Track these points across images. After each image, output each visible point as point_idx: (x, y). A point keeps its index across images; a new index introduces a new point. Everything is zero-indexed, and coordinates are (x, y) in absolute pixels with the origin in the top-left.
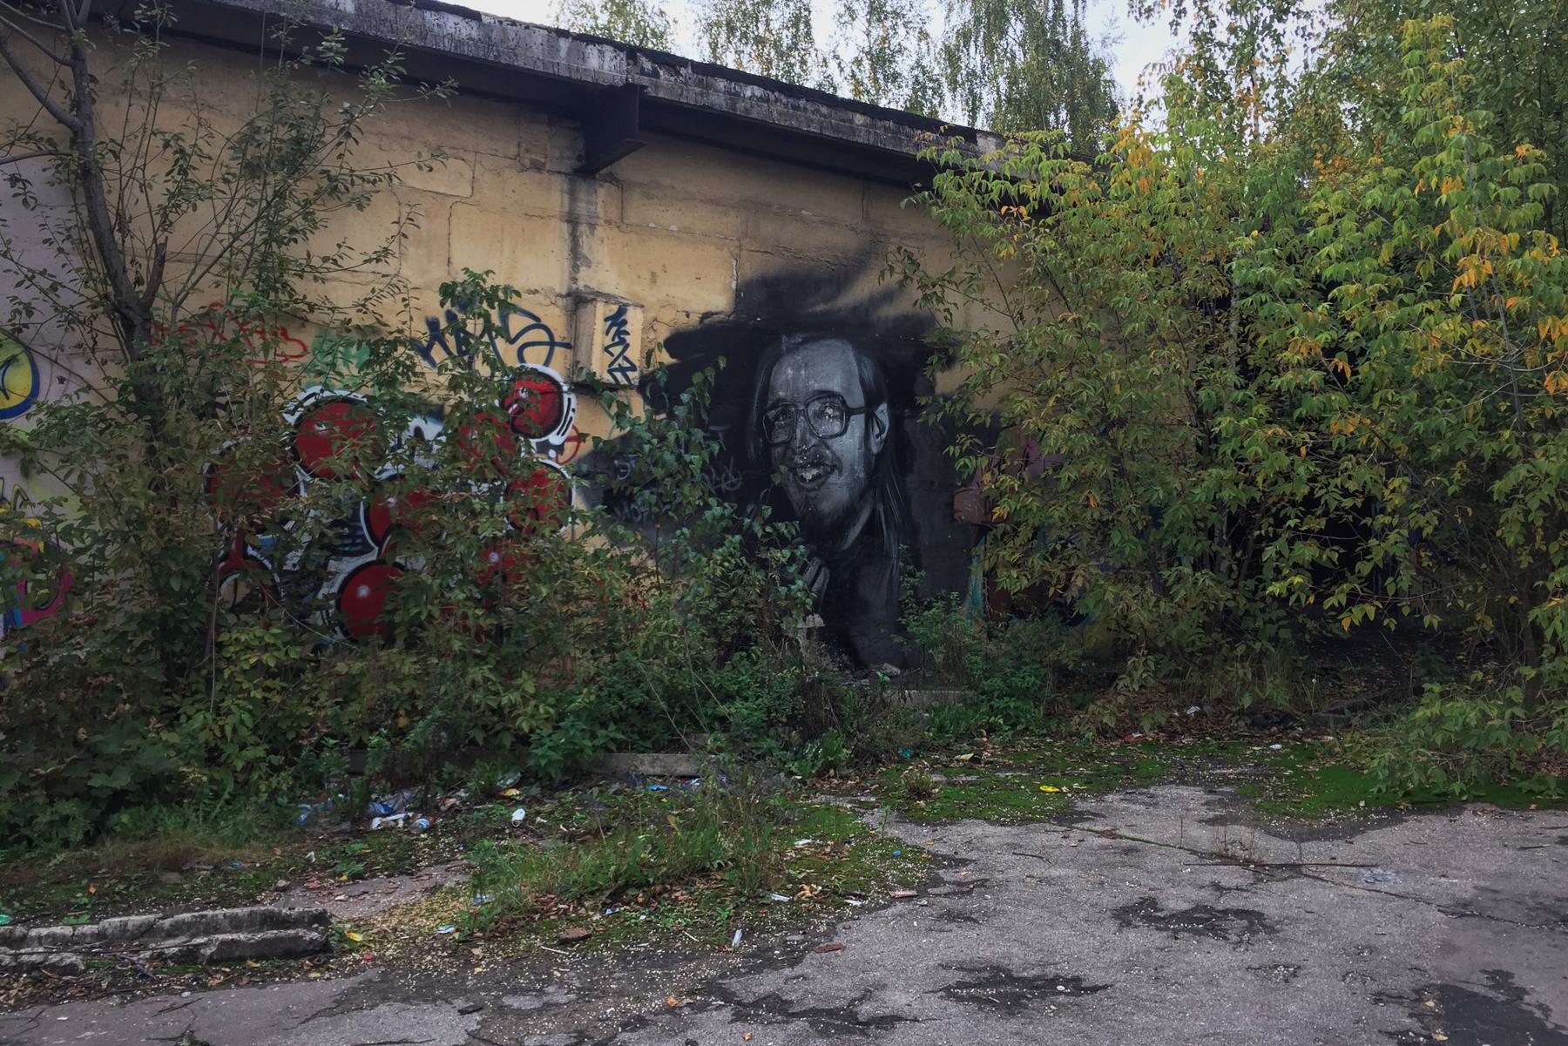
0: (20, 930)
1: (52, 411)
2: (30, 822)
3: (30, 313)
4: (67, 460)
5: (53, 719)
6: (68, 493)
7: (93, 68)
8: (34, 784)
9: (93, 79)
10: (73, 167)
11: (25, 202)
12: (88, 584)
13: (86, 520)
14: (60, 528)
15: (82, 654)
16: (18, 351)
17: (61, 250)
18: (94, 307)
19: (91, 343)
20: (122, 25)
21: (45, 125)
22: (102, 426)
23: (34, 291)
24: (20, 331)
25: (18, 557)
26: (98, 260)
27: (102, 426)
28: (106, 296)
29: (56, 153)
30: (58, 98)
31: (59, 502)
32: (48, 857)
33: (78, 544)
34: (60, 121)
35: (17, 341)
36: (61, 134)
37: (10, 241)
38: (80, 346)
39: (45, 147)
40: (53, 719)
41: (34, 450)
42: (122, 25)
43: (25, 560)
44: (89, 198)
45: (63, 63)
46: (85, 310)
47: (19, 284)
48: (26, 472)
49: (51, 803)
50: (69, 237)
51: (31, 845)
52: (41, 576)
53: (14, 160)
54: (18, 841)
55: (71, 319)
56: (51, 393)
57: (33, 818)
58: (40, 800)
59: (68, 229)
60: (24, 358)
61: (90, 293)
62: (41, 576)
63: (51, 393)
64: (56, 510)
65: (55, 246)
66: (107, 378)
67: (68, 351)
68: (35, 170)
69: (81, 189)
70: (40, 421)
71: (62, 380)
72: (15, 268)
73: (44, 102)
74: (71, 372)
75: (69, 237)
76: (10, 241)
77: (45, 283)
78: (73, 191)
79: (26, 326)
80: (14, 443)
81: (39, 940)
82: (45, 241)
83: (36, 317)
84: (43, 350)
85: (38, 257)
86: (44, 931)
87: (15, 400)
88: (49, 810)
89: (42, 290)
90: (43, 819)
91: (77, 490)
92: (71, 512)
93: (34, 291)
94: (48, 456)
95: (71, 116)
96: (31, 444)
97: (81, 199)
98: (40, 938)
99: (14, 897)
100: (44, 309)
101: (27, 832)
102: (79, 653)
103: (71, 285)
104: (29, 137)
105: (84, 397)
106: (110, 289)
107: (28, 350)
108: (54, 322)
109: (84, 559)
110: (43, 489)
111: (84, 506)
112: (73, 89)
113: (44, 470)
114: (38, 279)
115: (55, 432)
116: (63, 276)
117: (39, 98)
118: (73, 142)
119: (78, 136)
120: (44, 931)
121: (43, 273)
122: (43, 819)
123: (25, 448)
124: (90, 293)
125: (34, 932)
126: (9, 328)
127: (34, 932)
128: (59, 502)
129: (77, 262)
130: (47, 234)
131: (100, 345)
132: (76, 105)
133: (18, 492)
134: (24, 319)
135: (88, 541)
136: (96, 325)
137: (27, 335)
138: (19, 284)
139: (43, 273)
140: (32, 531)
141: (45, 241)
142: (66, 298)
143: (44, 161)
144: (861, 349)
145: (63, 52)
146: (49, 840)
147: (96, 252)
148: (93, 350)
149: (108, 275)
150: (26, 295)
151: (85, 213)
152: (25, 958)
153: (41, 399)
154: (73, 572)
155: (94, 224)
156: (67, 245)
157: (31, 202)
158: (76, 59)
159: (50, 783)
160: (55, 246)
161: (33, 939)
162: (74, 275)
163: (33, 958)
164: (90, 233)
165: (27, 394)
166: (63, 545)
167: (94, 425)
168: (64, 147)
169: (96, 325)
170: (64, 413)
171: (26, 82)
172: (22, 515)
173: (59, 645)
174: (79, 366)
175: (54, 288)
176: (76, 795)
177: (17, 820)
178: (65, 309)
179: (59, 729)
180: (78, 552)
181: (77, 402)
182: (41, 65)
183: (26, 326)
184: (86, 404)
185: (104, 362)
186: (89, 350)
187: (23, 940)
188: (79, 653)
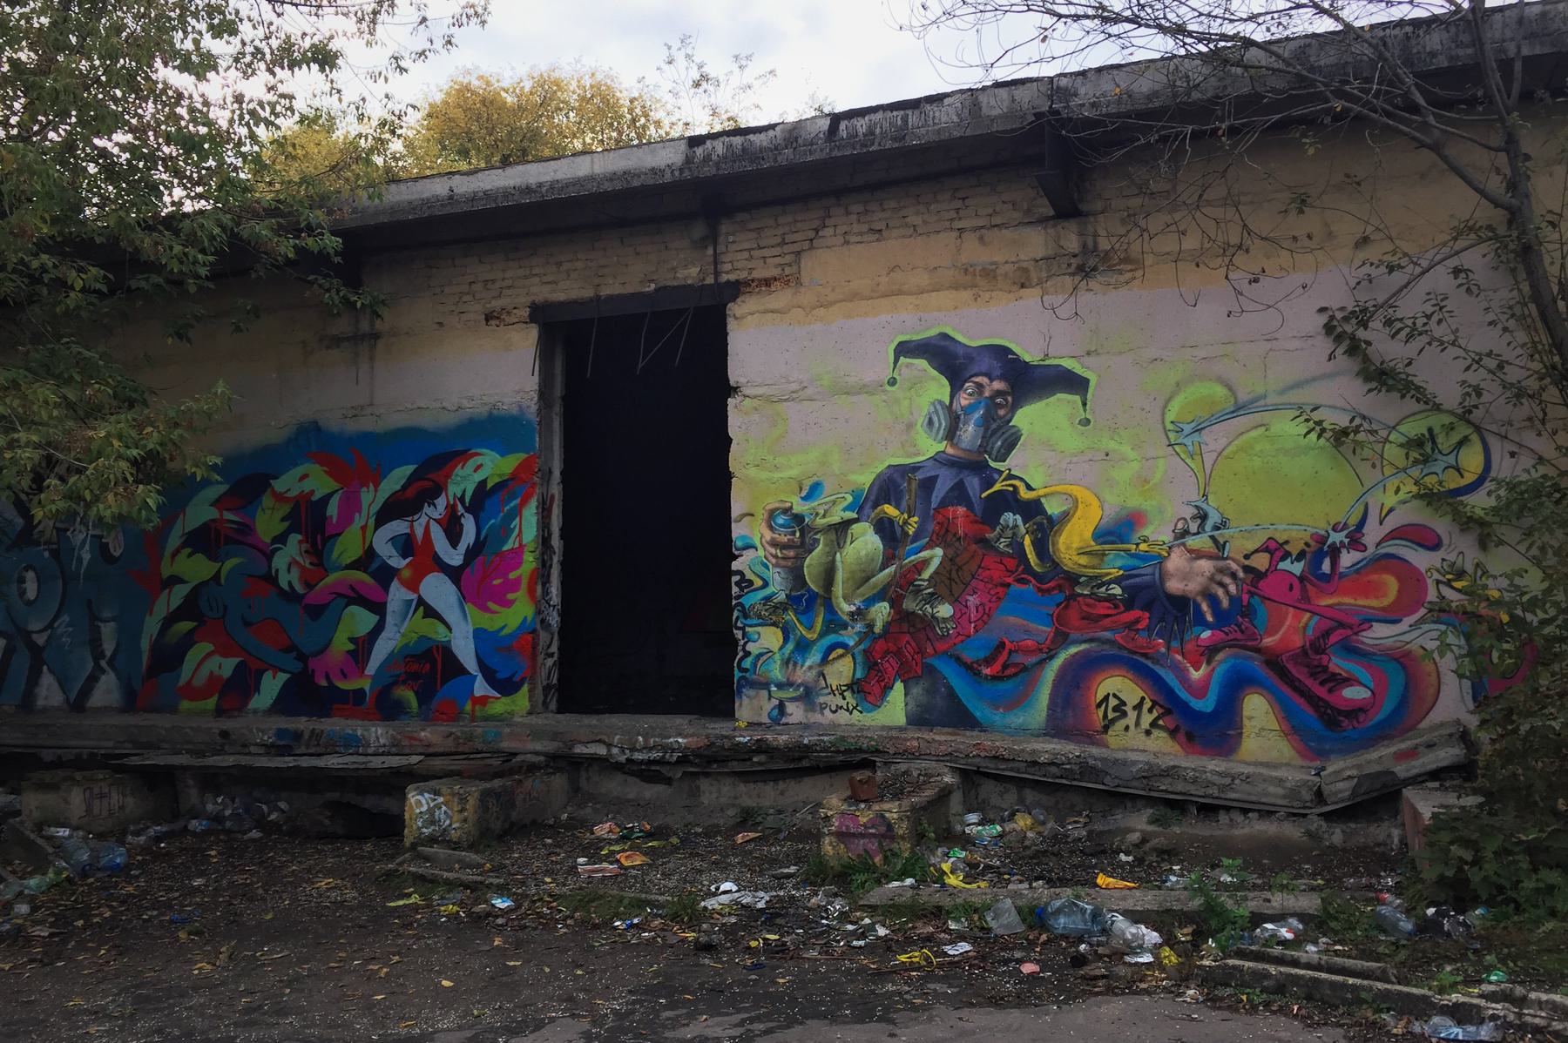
0: (1519, 991)
1: (1512, 487)
2: (1516, 885)
3: (1479, 394)
4: (1528, 533)
5: (1530, 786)
6: (1526, 564)
7: (1526, 146)
8: (1516, 849)
9: (1527, 157)
10: (1512, 246)
11: (1468, 290)
12: (1556, 655)
13: (1547, 592)
14: (1525, 598)
15: (1556, 725)
16: (1469, 431)
17: (1505, 330)
18: (1541, 379)
19: (1541, 415)
20: (1554, 95)
21: (1486, 214)
22: (1557, 495)
23: (1482, 372)
24: (1470, 412)
25: (1484, 627)
26: (1541, 332)
27: (1557, 495)
28: (1554, 367)
29: (1496, 238)
30: (1495, 185)
31: (1520, 573)
32: (1537, 923)
33: (1541, 615)
34: (1497, 205)
35: (1468, 422)
36: (1499, 217)
37: (1457, 330)
38: (1530, 419)
39: (1485, 234)
40: (1530, 786)
41: (1490, 524)
42: (1554, 95)
43: (1491, 630)
44: (1530, 273)
45: (1497, 150)
46: (1533, 384)
47: (1468, 369)
48: (1483, 545)
49: (1535, 870)
50: (1513, 315)
51: (1518, 909)
52: (1506, 646)
53: (1457, 253)
54: (1507, 901)
55: (1520, 393)
56: (1504, 468)
57: (1519, 882)
58: (1525, 866)
59: (1511, 308)
60: (1475, 438)
61: (1537, 366)
62: (1506, 646)
63: (1504, 468)
64: (1517, 581)
65: (1500, 326)
66: (1559, 448)
67: (1517, 425)
68: (1476, 259)
69: (1521, 267)
70: (1498, 497)
71: (1513, 454)
72: (1462, 353)
73: (1481, 192)
74: (1521, 446)
75: (1513, 315)
76: (1457, 330)
77: (1492, 363)
78: (1513, 270)
79: (1476, 407)
80: (1470, 519)
81: (1540, 1004)
82: (1490, 324)
83: (1486, 397)
84: (1494, 428)
85: (1485, 340)
86: (1544, 997)
87: (1470, 478)
88: (1534, 877)
89: (1490, 371)
90: (1529, 884)
91: (1537, 562)
92: (1534, 582)
93: (1482, 372)
94: (1504, 529)
95: (1506, 198)
96: (1488, 519)
97: (1522, 275)
98: (1540, 1002)
99: (1509, 955)
100: (1492, 388)
101: (1514, 895)
102: (1553, 723)
103: (1517, 362)
104: (1471, 229)
105: (1542, 470)
106: (1557, 359)
107: (1478, 429)
108: (1502, 400)
109: (1548, 630)
110: (1501, 562)
111: (1547, 576)
112: (1508, 172)
113: (1501, 543)
114: (1487, 361)
115: (1515, 507)
116: (1508, 355)
117: (1477, 190)
118: (1510, 223)
119: (1515, 216)
120: (1544, 997)
121: (1489, 354)
122: (1529, 884)
123: (1482, 523)
124: (1537, 366)
125: (1533, 995)
126: (1460, 411)
127: (1533, 995)
128: (1520, 573)
129: (1521, 337)
130: (1491, 317)
131: (1550, 415)
132: (1512, 186)
133: (1477, 565)
134: (1473, 400)
135: (1552, 612)
136: (1545, 396)
137: (1477, 415)
138: (1468, 369)
139: (1489, 354)
140: (1499, 603)
141: (1490, 324)
142: (1513, 374)
143: (1483, 248)
144: (404, 682)
145: (1497, 139)
146: (1536, 906)
147: (1539, 324)
148: (1543, 422)
149: (1554, 344)
150: (1473, 378)
151: (1525, 288)
152: (1529, 1019)
153: (1493, 474)
154: (1539, 642)
155: (1537, 297)
156: (1512, 324)
157: (1474, 289)
158: (1510, 145)
159: (1531, 849)
160: (1500, 326)
161: (1533, 1001)
162: (1519, 351)
163: (1537, 1021)
164: (1532, 307)
165: (1480, 470)
166: (1529, 617)
167: (1549, 495)
168: (1502, 230)
169: (1545, 396)
170: (1523, 487)
171: (1464, 178)
172: (1485, 587)
173: (1531, 714)
174: (1529, 438)
175: (1500, 367)
176: (1558, 866)
177: (1503, 882)
178: (1512, 385)
179: (1537, 798)
180: (1544, 623)
181: (1534, 475)
182: (1475, 157)
183: (1476, 407)
184: (1544, 476)
185: (1555, 432)
186: (1538, 422)
187: (1521, 1002)
188: (1553, 723)
